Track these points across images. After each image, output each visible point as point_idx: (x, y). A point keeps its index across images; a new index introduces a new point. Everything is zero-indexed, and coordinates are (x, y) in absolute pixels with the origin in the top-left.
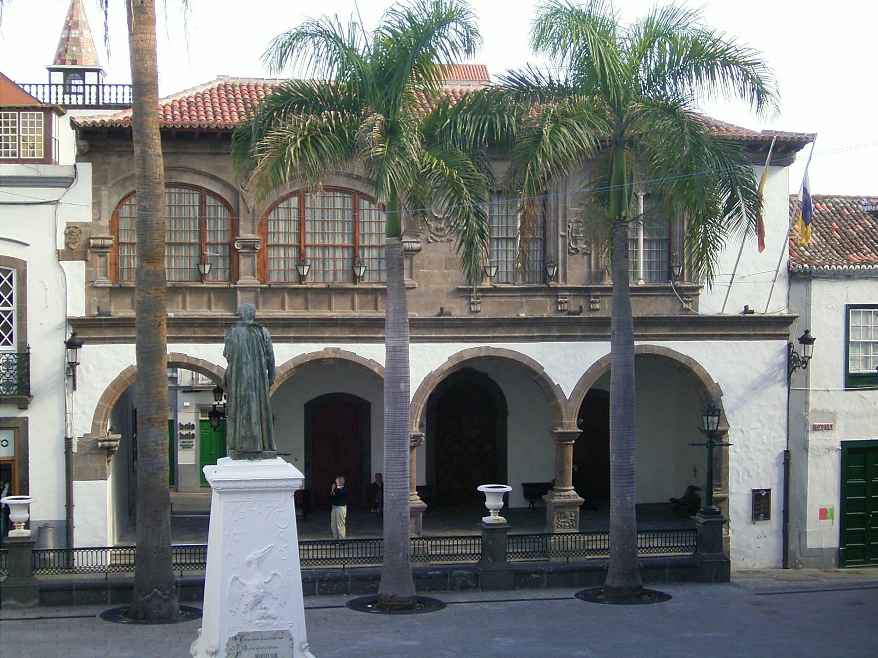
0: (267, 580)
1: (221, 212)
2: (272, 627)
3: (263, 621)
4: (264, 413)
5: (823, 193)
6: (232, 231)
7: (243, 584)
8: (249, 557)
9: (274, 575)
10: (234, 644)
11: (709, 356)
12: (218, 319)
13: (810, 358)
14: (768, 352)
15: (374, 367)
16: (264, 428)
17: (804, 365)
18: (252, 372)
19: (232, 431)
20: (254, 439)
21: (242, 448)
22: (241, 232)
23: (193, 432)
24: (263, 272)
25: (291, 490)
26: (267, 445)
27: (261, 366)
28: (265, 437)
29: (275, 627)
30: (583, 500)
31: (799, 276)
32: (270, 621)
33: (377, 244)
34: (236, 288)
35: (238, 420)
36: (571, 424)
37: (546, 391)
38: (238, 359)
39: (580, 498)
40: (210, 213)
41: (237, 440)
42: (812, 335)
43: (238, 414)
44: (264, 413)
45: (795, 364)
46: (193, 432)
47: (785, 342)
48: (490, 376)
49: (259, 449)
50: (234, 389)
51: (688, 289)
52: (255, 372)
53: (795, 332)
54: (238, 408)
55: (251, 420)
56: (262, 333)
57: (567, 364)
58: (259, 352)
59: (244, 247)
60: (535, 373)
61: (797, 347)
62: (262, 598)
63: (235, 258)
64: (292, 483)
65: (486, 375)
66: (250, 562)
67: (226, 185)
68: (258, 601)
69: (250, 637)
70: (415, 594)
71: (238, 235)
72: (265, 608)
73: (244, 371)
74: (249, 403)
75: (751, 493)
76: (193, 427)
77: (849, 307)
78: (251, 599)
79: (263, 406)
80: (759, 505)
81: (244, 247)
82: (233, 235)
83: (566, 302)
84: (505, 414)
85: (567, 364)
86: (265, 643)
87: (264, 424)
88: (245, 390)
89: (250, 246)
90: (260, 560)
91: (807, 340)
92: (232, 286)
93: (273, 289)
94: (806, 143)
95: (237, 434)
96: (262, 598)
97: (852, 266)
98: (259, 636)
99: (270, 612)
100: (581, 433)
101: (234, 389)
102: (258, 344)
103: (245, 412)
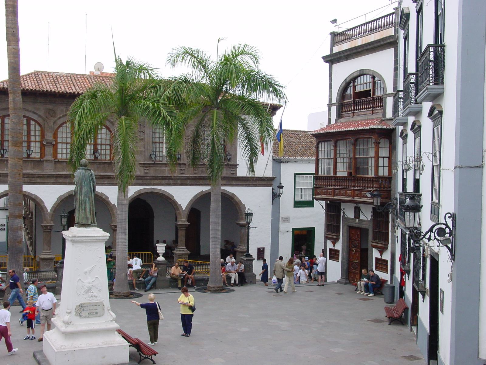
0: (93, 280)
1: (38, 128)
2: (95, 300)
3: (92, 298)
4: (91, 207)
5: (287, 129)
6: (42, 136)
7: (83, 282)
8: (86, 270)
9: (97, 278)
10: (79, 309)
11: (241, 193)
12: (35, 174)
13: (282, 194)
14: (267, 191)
15: (103, 196)
16: (92, 214)
17: (279, 197)
18: (87, 189)
19: (78, 215)
20: (87, 218)
21: (82, 222)
22: (46, 137)
23: (4, 227)
24: (55, 154)
25: (103, 241)
26: (92, 222)
27: (91, 187)
28: (92, 218)
29: (97, 300)
30: (190, 252)
31: (277, 162)
32: (94, 298)
33: (105, 143)
34: (43, 161)
35: (80, 210)
36: (183, 220)
37: (175, 207)
38: (80, 184)
39: (189, 252)
40: (33, 128)
41: (80, 219)
42: (282, 185)
43: (80, 208)
44: (91, 207)
45: (275, 196)
46: (4, 227)
47: (271, 188)
48: (147, 201)
49: (90, 223)
50: (78, 197)
51: (233, 165)
52: (88, 189)
53: (275, 184)
54: (81, 205)
55: (86, 210)
56: (91, 173)
57: (184, 196)
58: (90, 181)
59: (47, 143)
60: (171, 199)
61: (277, 190)
62: (91, 288)
63: (43, 148)
64: (105, 238)
65: (145, 201)
66: (86, 272)
67: (40, 116)
68: (89, 290)
69: (86, 305)
70: (130, 291)
71: (44, 138)
72: (92, 293)
73: (83, 189)
74: (85, 203)
75: (257, 249)
76: (4, 225)
77: (296, 174)
78: (86, 288)
79: (91, 204)
80: (260, 254)
81: (47, 143)
82: (42, 138)
83: (184, 170)
84: (153, 217)
85: (184, 196)
86: (91, 308)
87: (92, 212)
88: (84, 197)
89: (49, 142)
90: (90, 271)
91: (281, 187)
92: (42, 160)
93: (60, 161)
94: (281, 107)
95: (80, 216)
96: (91, 288)
97: (297, 158)
98: (89, 305)
99: (95, 294)
100: (189, 225)
101: (78, 197)
102: (89, 177)
103: (83, 207)
